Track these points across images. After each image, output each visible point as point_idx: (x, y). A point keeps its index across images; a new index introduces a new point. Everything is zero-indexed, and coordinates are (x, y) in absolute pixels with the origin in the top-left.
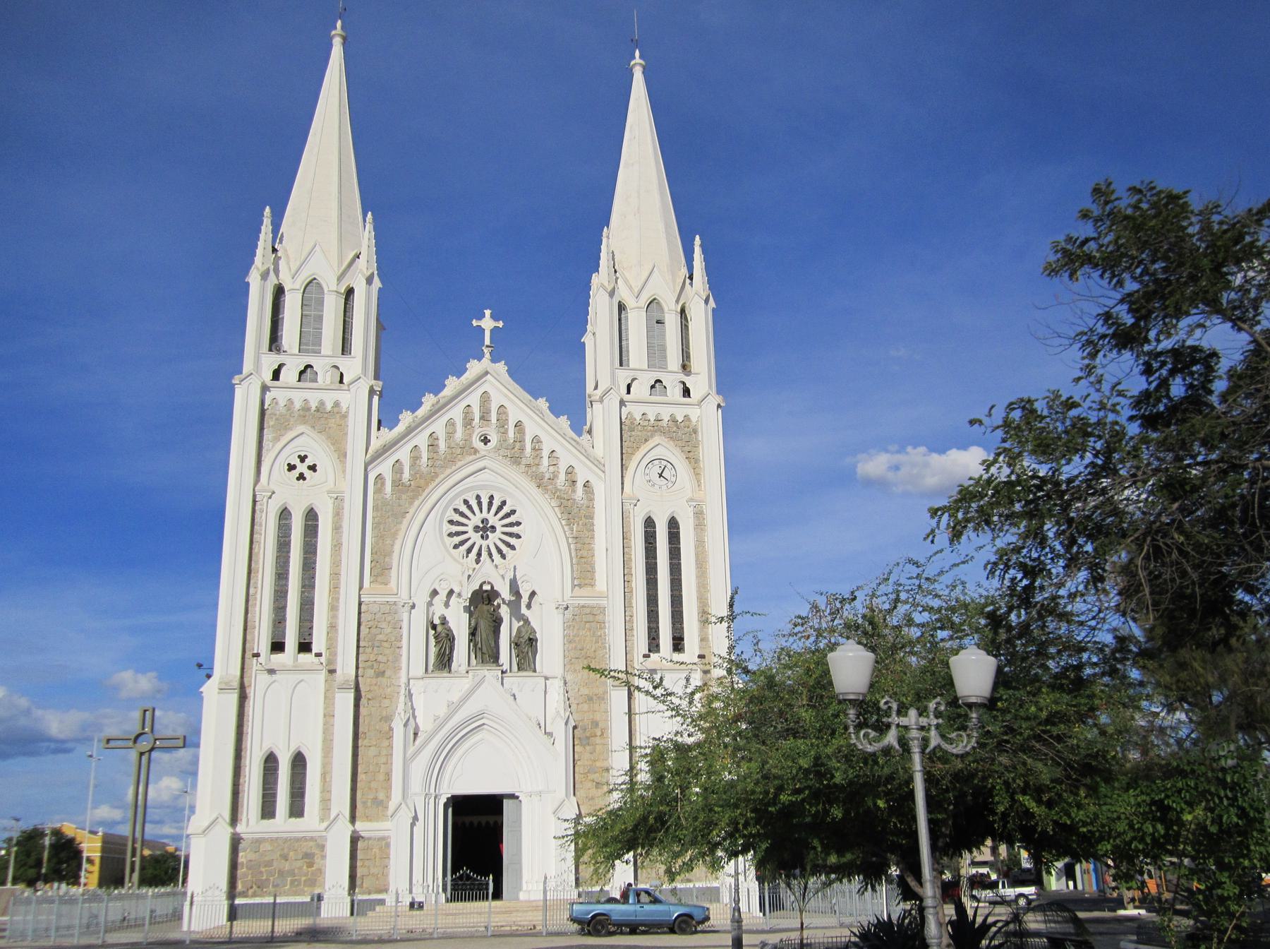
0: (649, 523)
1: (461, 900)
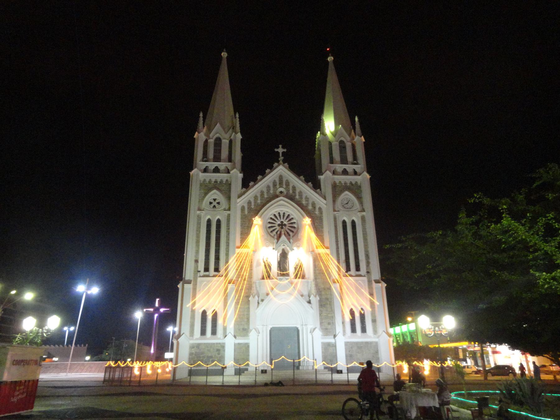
0: (204, 313)
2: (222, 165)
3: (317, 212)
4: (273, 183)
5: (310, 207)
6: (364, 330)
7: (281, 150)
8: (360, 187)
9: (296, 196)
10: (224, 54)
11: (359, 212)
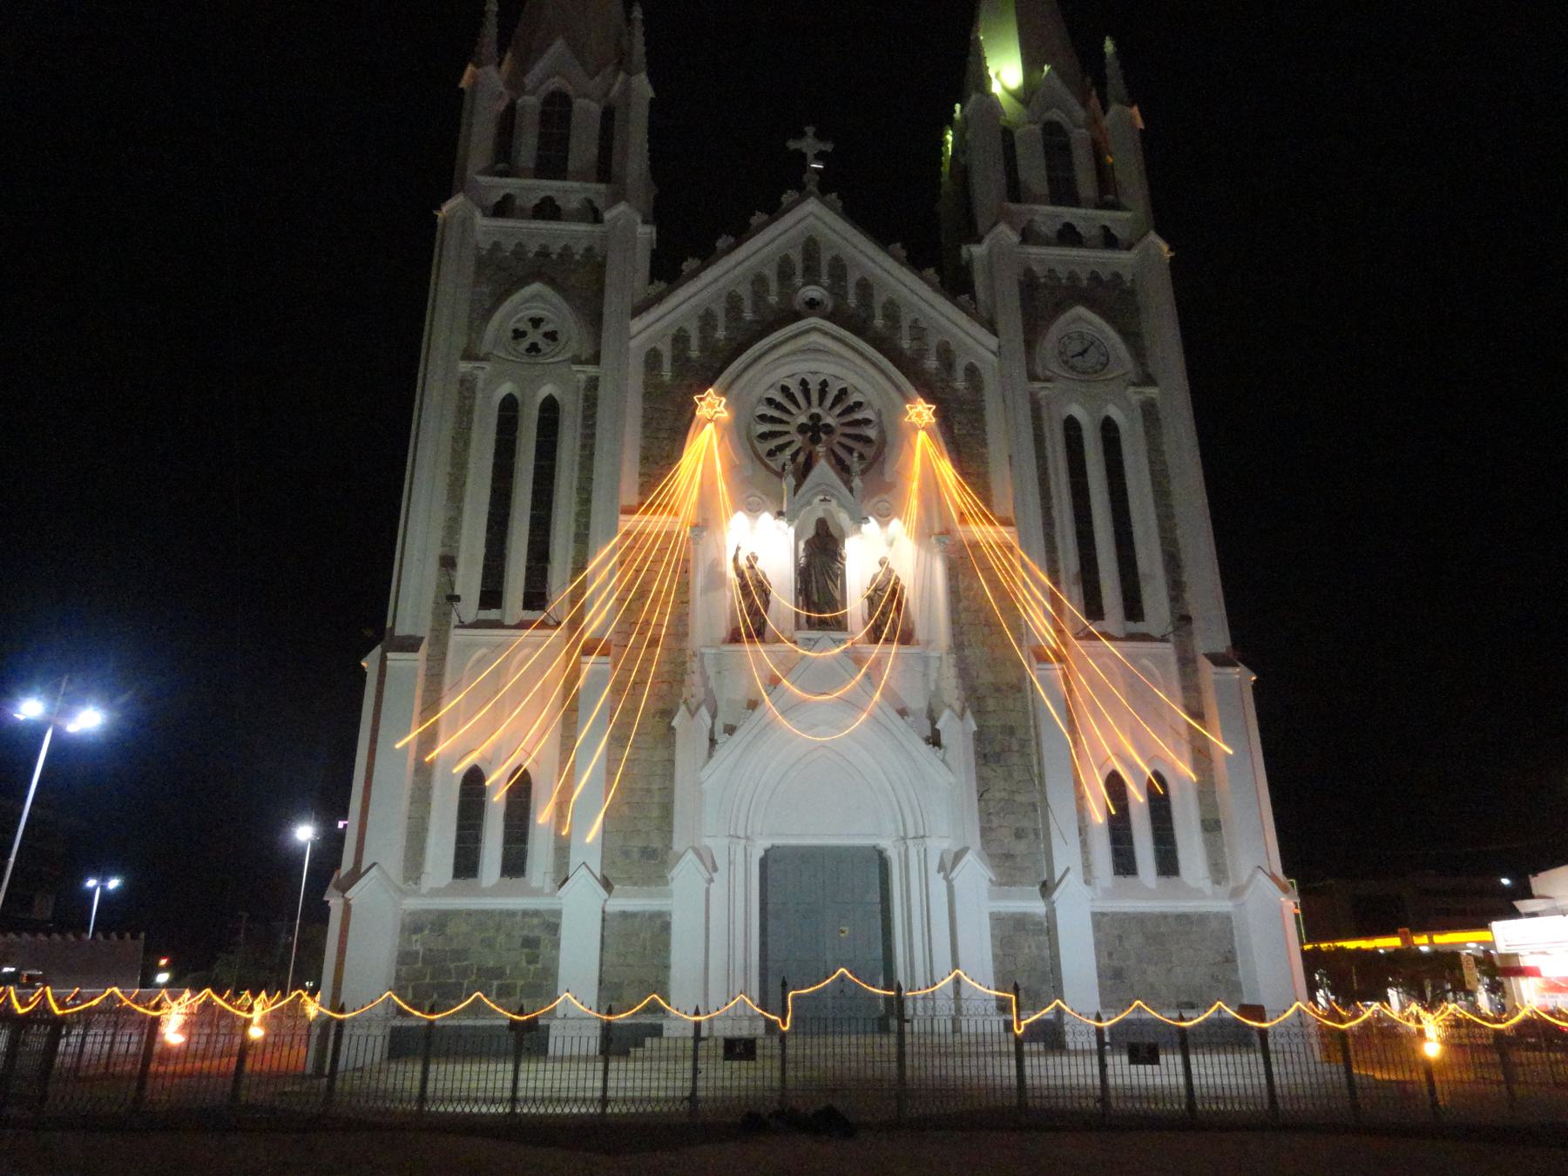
0: (474, 781)
3: (960, 384)
5: (932, 363)
6: (1168, 864)
7: (809, 144)
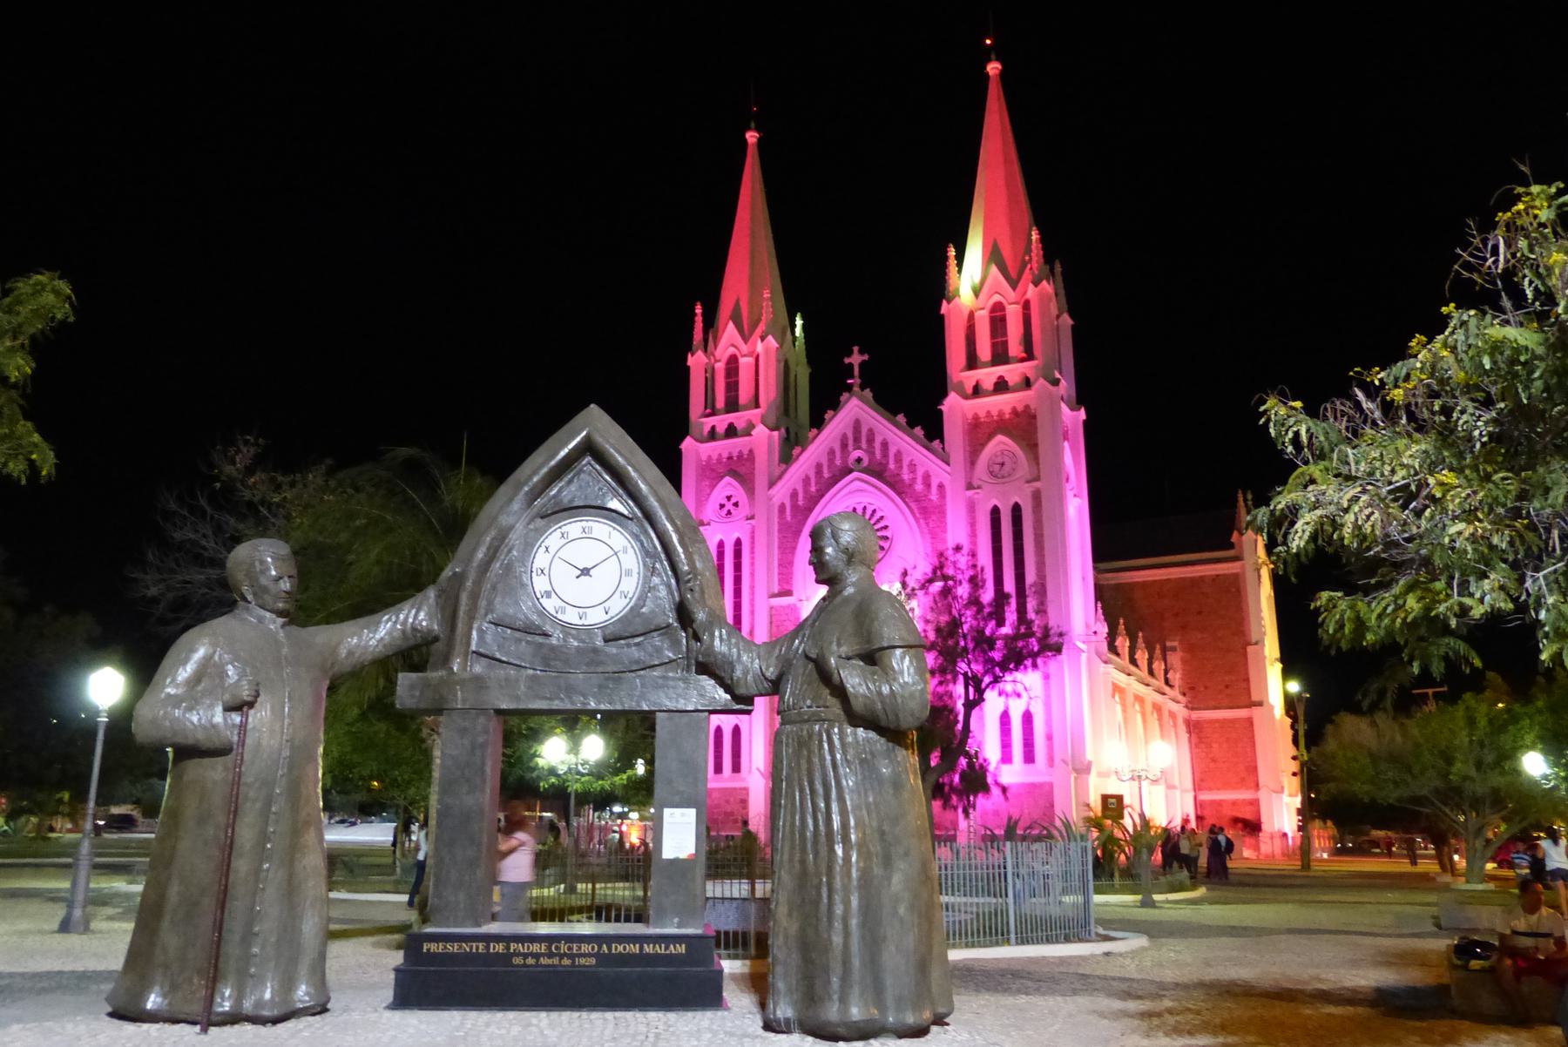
1: (1001, 896)
2: (739, 419)
3: (934, 495)
4: (842, 440)
5: (919, 487)
8: (1034, 417)
9: (888, 463)
10: (752, 137)
11: (1028, 482)
